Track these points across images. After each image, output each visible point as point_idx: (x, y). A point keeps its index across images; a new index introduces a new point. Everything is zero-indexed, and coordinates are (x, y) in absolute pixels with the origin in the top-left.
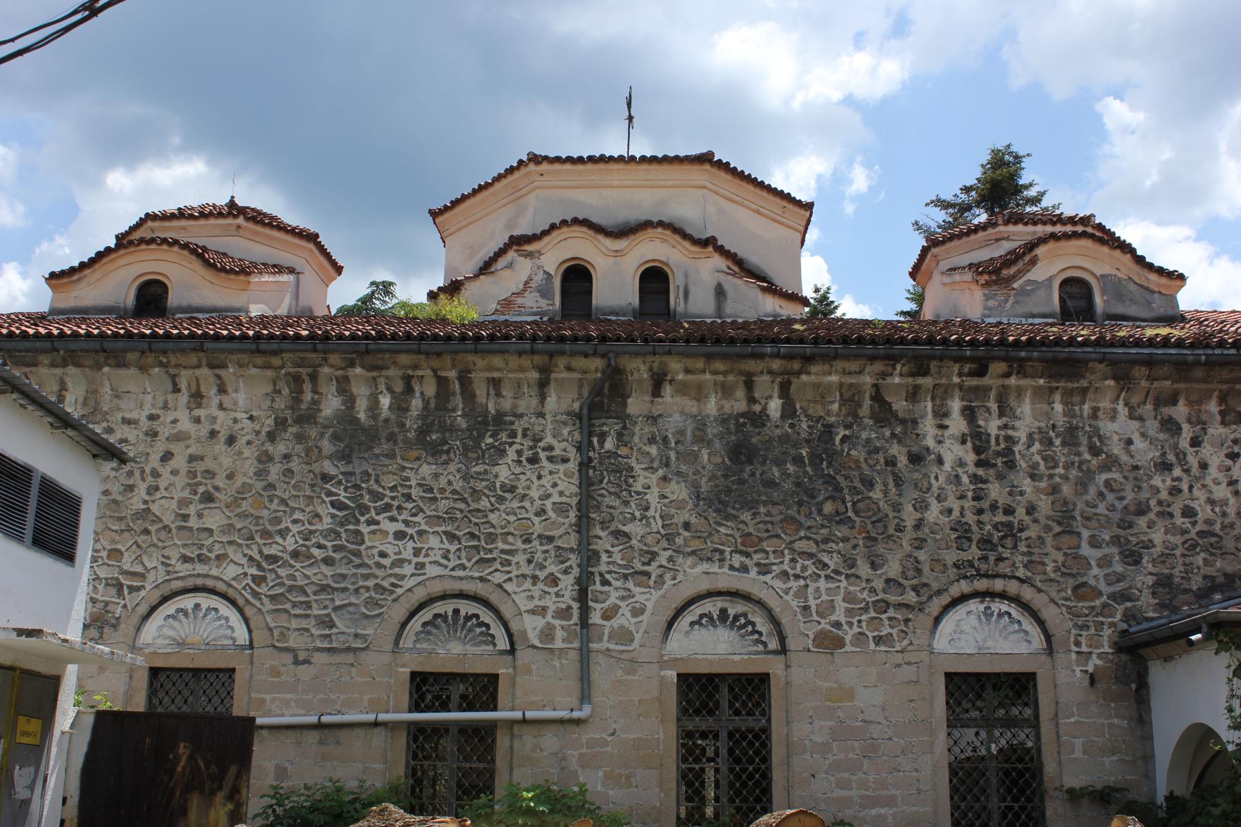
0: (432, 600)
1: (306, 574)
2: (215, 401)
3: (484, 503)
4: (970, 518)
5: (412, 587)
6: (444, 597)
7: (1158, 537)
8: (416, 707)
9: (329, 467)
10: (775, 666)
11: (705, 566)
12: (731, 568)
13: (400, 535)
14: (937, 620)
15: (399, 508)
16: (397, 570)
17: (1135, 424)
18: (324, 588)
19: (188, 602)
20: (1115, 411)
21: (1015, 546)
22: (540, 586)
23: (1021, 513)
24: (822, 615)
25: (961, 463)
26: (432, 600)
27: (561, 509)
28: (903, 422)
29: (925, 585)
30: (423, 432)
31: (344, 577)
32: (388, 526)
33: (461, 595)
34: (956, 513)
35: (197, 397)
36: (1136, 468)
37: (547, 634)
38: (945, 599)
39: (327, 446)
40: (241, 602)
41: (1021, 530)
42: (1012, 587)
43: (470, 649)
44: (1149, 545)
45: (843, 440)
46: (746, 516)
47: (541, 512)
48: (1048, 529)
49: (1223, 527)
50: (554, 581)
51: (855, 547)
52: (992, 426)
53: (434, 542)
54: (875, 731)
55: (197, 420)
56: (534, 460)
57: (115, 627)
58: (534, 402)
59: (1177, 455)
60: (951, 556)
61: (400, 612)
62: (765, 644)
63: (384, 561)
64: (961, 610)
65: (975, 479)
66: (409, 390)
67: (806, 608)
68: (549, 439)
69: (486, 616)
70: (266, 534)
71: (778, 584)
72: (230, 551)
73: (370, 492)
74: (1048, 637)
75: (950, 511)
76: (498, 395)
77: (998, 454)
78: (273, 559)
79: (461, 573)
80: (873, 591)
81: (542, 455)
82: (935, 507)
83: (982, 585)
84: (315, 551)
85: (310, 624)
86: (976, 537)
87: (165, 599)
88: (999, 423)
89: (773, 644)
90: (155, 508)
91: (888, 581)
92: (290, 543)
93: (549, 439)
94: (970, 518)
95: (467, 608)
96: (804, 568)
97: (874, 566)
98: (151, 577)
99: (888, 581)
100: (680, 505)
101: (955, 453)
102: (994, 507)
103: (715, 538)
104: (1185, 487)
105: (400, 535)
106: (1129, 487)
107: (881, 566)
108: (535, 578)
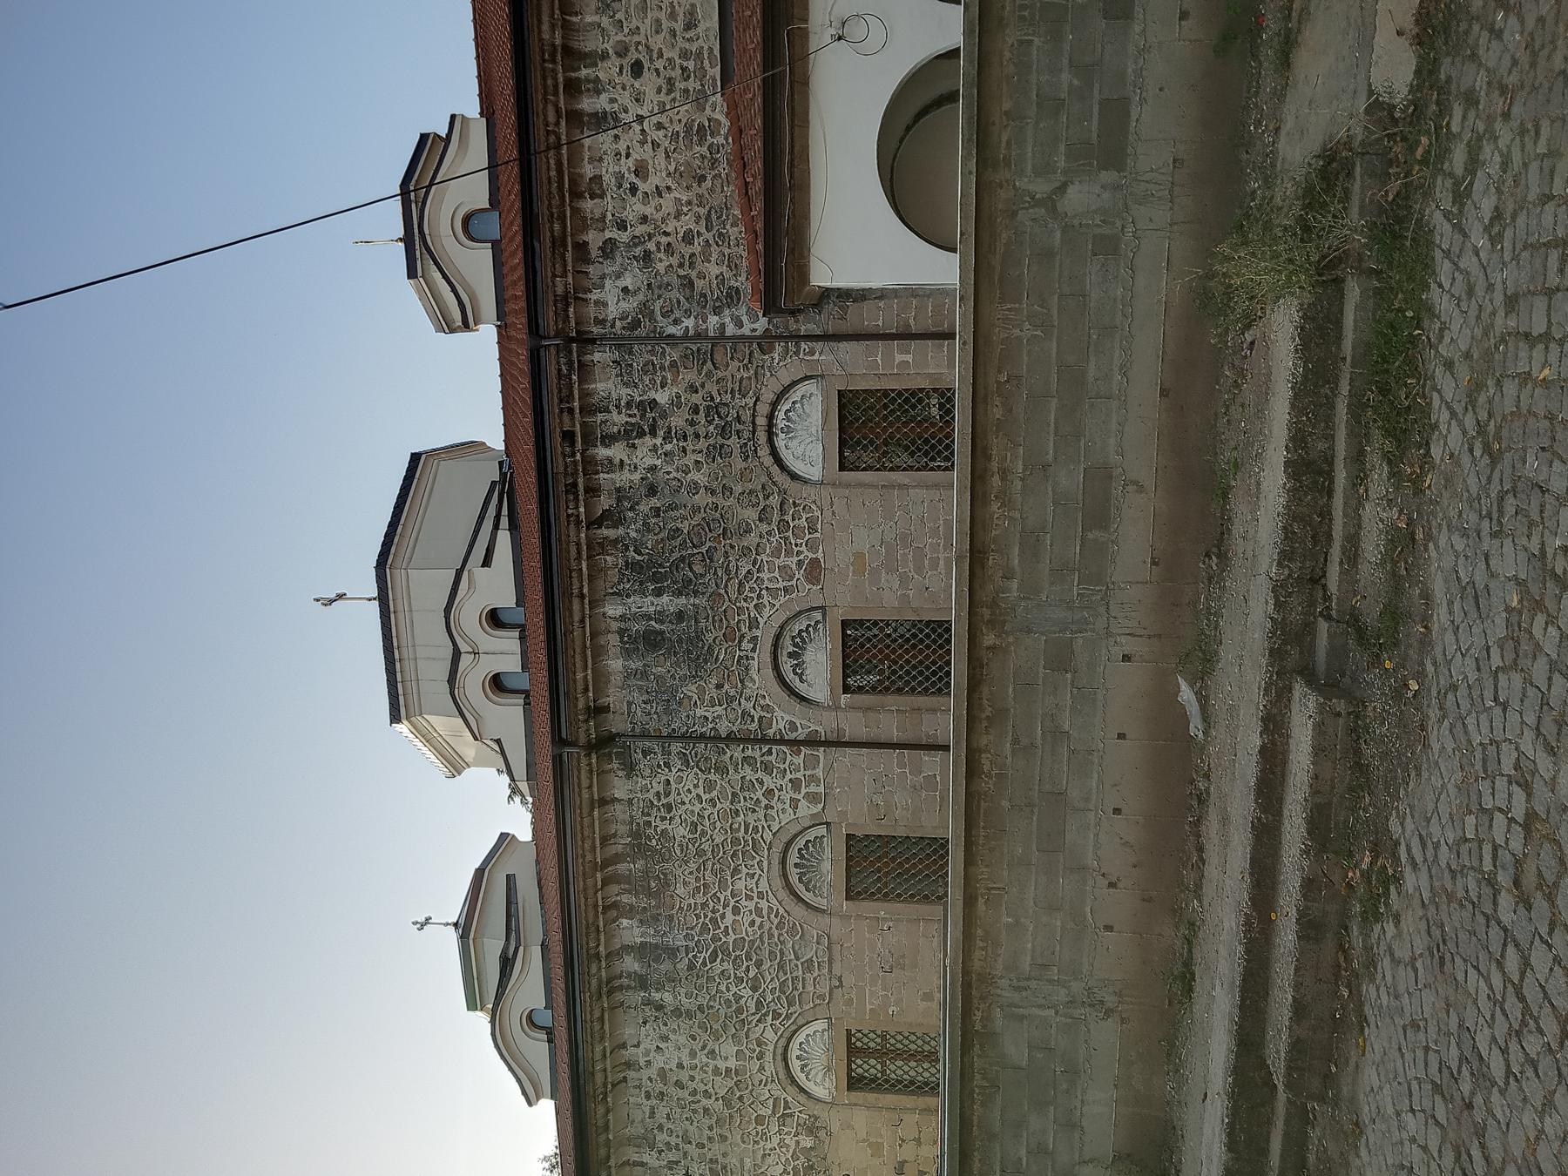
0: (788, 886)
1: (770, 982)
2: (633, 1050)
3: (707, 847)
4: (702, 444)
5: (777, 901)
6: (785, 875)
7: (714, 270)
8: (943, 690)
9: (682, 965)
10: (838, 615)
11: (753, 673)
12: (754, 650)
13: (736, 911)
14: (794, 477)
15: (713, 912)
16: (765, 912)
17: (608, 283)
18: (781, 967)
19: (795, 1065)
20: (597, 303)
21: (726, 405)
22: (773, 803)
23: (696, 399)
24: (791, 578)
25: (654, 449)
26: (788, 886)
27: (710, 786)
28: (619, 500)
29: (763, 487)
30: (650, 895)
31: (771, 952)
32: (730, 917)
33: (783, 862)
34: (700, 458)
35: (628, 1065)
36: (649, 285)
37: (813, 798)
38: (775, 469)
39: (665, 966)
40: (793, 1028)
41: (712, 399)
42: (763, 409)
43: (828, 851)
44: (721, 279)
45: (640, 554)
46: (709, 637)
47: (712, 802)
48: (709, 375)
49: (700, 205)
50: (769, 793)
51: (732, 547)
52: (618, 419)
53: (740, 885)
54: (889, 537)
55: (649, 1063)
56: (669, 808)
57: (816, 1118)
58: (617, 806)
59: (636, 245)
60: (738, 464)
61: (799, 911)
62: (817, 622)
63: (758, 921)
64: (785, 455)
65: (667, 438)
66: (615, 905)
67: (786, 590)
68: (650, 795)
69: (800, 842)
70: (739, 1011)
71: (767, 612)
72: (753, 1036)
73: (701, 934)
74: (807, 378)
75: (697, 462)
76: (615, 835)
77: (643, 416)
78: (759, 1004)
79: (765, 864)
80: (769, 533)
81: (664, 801)
82: (694, 476)
83: (762, 437)
84: (751, 975)
85: (809, 978)
86: (720, 440)
87: (793, 1081)
88: (615, 413)
89: (818, 616)
90: (722, 1093)
91: (760, 520)
92: (746, 993)
93: (650, 795)
94: (702, 444)
95: (793, 858)
96: (752, 590)
97: (748, 531)
98: (776, 1093)
99: (760, 520)
100: (701, 691)
101: (644, 454)
102: (692, 423)
103: (729, 664)
104: (664, 240)
105: (736, 911)
106: (667, 295)
107: (748, 524)
108: (766, 807)
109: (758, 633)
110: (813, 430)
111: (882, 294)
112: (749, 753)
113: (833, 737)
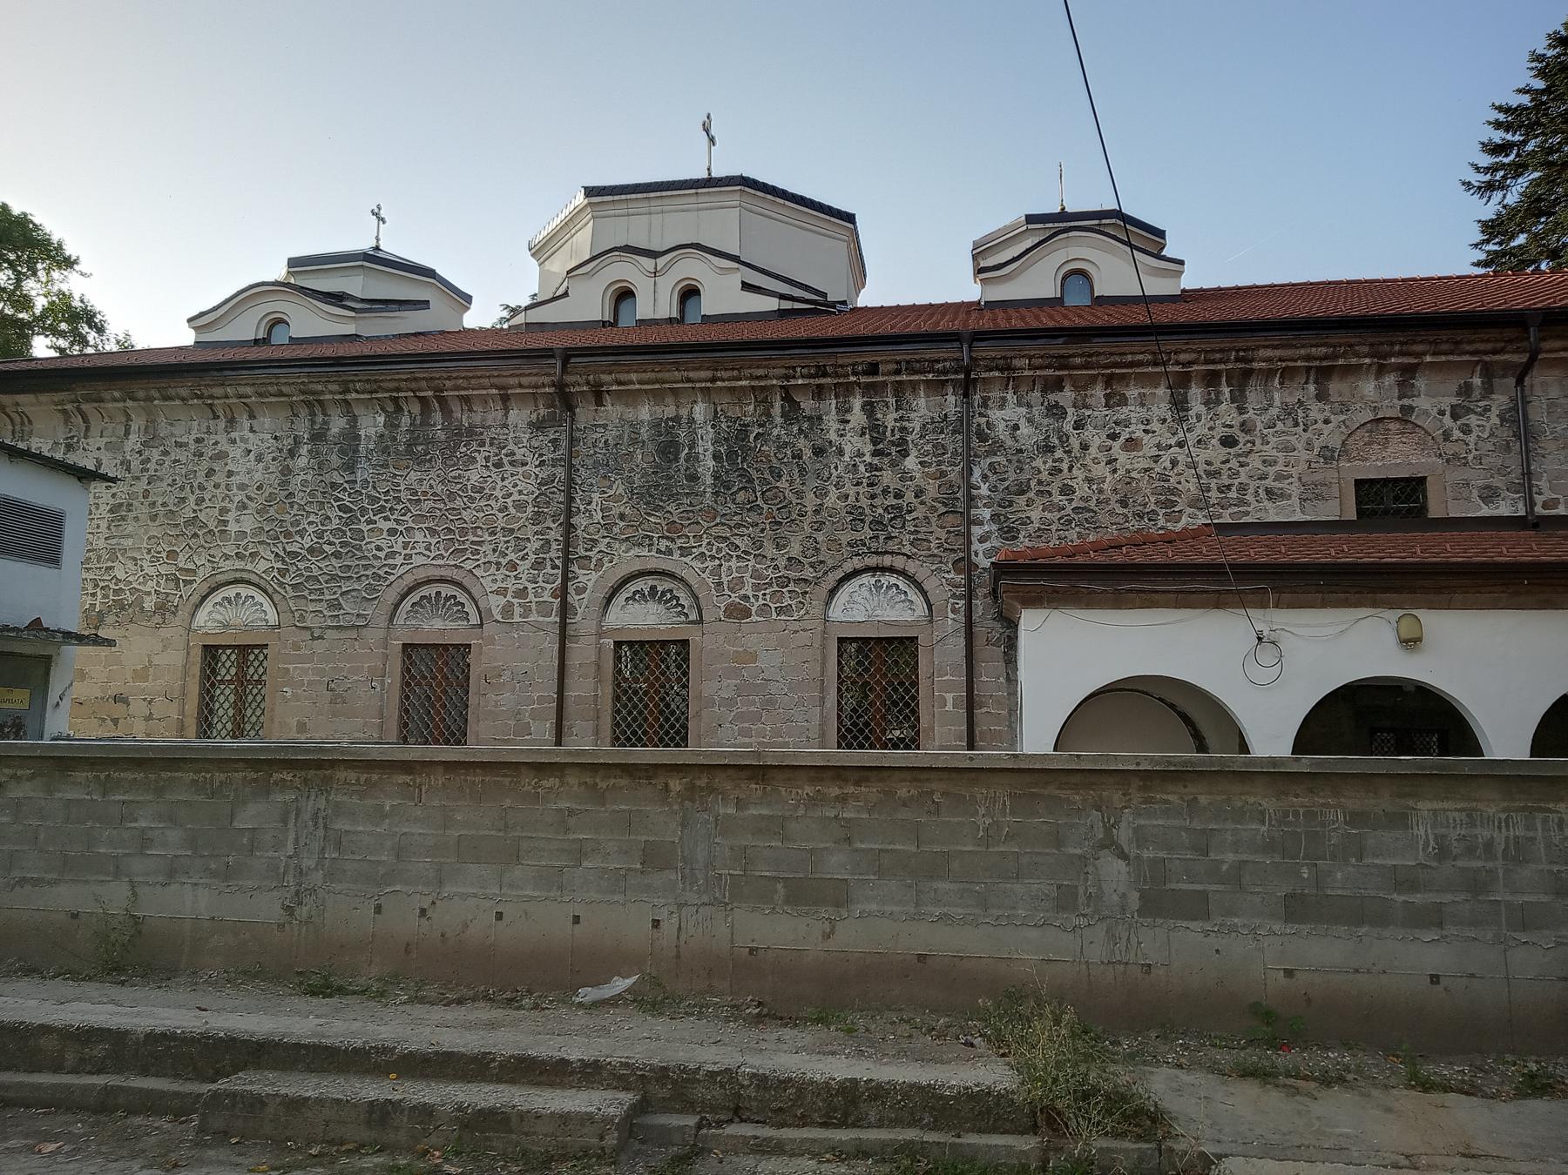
10: (693, 635)
11: (635, 551)
12: (658, 551)
42: (899, 562)
51: (762, 531)
62: (686, 615)
74: (930, 606)
89: (693, 616)
109: (676, 556)
110: (878, 612)
111: (1012, 681)
112: (554, 546)
113: (570, 631)
